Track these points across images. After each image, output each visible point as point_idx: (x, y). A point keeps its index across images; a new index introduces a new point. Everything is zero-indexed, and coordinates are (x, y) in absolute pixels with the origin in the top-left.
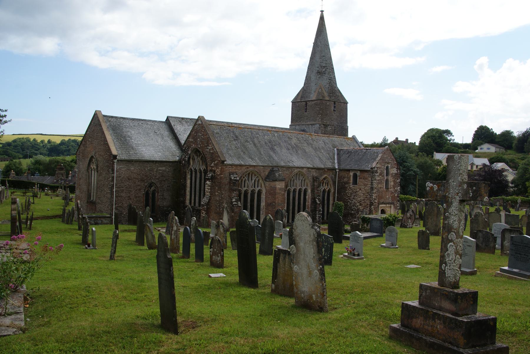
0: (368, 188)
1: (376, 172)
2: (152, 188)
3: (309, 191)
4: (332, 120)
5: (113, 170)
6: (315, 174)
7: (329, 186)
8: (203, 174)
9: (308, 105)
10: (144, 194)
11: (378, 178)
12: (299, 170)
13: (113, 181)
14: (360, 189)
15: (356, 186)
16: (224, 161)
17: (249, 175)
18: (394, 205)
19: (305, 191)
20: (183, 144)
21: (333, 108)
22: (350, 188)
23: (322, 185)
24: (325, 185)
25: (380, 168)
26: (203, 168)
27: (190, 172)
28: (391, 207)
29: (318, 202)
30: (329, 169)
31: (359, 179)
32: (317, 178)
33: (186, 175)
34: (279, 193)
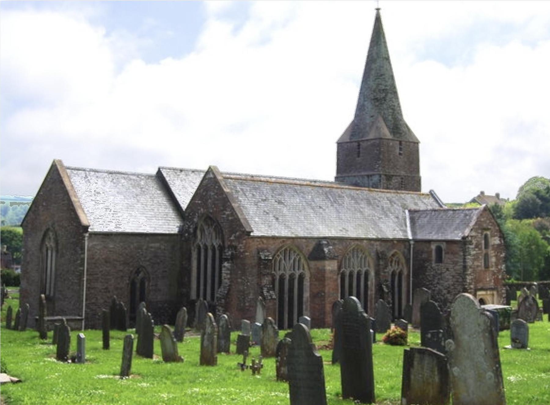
0: (459, 267)
1: (471, 243)
2: (141, 275)
3: (372, 274)
4: (398, 169)
5: (83, 249)
6: (378, 246)
7: (400, 266)
8: (217, 252)
9: (361, 147)
10: (128, 284)
11: (473, 253)
12: (356, 242)
13: (82, 265)
14: (448, 269)
15: (440, 264)
16: (250, 232)
17: (287, 252)
18: (498, 292)
19: (367, 274)
20: (184, 210)
21: (398, 151)
22: (432, 268)
23: (389, 264)
24: (395, 264)
25: (475, 237)
26: (216, 243)
27: (196, 250)
28: (493, 295)
29: (386, 290)
30: (400, 241)
31: (446, 253)
32: (383, 253)
33: (191, 253)
34: (330, 278)
